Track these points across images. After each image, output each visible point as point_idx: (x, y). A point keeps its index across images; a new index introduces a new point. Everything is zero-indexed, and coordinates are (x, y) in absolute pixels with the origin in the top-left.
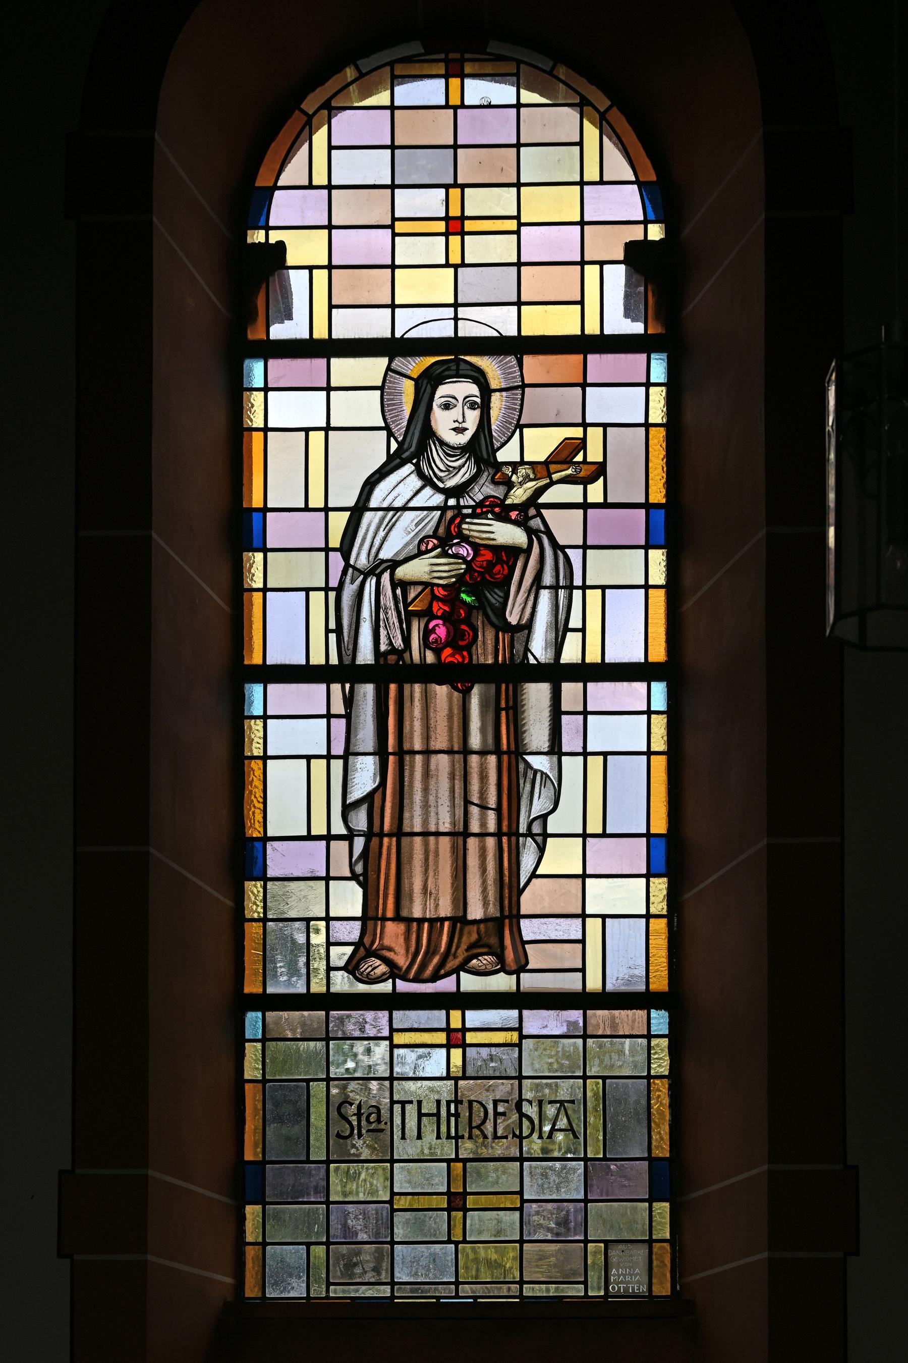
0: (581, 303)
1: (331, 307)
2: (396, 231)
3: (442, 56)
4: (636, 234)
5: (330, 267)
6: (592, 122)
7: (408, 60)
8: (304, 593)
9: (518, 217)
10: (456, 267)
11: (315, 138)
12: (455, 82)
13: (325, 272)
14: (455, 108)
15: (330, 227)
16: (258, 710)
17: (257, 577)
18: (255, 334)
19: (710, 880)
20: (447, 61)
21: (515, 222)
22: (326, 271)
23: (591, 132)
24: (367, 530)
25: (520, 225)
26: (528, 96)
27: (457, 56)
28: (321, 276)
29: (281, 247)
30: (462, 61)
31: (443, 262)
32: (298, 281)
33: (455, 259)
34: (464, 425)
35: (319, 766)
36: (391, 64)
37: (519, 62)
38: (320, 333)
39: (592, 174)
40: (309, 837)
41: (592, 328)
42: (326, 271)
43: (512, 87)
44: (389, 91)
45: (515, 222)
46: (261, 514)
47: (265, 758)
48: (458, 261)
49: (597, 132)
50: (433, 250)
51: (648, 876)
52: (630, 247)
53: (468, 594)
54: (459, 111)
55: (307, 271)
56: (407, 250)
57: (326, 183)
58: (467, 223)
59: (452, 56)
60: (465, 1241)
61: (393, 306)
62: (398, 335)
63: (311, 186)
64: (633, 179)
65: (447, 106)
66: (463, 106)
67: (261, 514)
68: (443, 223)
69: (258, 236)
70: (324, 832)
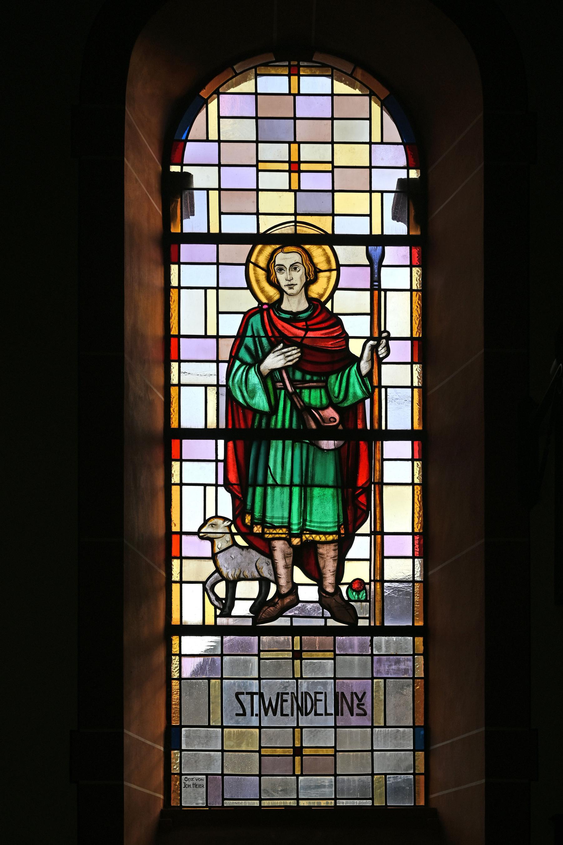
0: (370, 215)
1: (219, 117)
2: (259, 169)
3: (287, 63)
4: (403, 174)
5: (220, 189)
6: (376, 103)
7: (266, 65)
8: (206, 192)
9: (332, 162)
10: (295, 191)
11: (210, 106)
12: (294, 79)
13: (217, 192)
14: (294, 95)
15: (218, 264)
16: (416, 390)
17: (174, 284)
18: (175, 229)
19: (442, 207)
20: (290, 66)
21: (330, 165)
22: (215, 291)
23: (376, 109)
24: (239, 421)
25: (334, 167)
26: (341, 88)
27: (296, 63)
28: (214, 195)
29: (188, 177)
30: (299, 66)
31: (288, 188)
32: (199, 198)
33: (295, 186)
34: (292, 282)
35: (211, 490)
36: (255, 67)
37: (333, 68)
38: (214, 229)
39: (376, 138)
40: (206, 336)
41: (377, 231)
42: (215, 291)
43: (329, 79)
44: (254, 80)
45: (330, 165)
46: (177, 339)
47: (179, 288)
48: (296, 92)
49: (379, 109)
50: (282, 180)
51: (412, 363)
52: (401, 182)
53: (303, 427)
54: (297, 97)
55: (203, 291)
56: (266, 180)
57: (217, 138)
58: (302, 165)
59: (292, 63)
60: (302, 678)
61: (258, 214)
62: (262, 231)
63: (207, 140)
64: (401, 141)
65: (290, 94)
66: (299, 94)
67: (177, 339)
68: (287, 165)
69: (175, 169)
70: (215, 334)
